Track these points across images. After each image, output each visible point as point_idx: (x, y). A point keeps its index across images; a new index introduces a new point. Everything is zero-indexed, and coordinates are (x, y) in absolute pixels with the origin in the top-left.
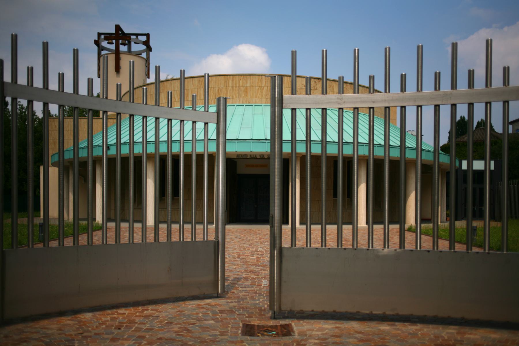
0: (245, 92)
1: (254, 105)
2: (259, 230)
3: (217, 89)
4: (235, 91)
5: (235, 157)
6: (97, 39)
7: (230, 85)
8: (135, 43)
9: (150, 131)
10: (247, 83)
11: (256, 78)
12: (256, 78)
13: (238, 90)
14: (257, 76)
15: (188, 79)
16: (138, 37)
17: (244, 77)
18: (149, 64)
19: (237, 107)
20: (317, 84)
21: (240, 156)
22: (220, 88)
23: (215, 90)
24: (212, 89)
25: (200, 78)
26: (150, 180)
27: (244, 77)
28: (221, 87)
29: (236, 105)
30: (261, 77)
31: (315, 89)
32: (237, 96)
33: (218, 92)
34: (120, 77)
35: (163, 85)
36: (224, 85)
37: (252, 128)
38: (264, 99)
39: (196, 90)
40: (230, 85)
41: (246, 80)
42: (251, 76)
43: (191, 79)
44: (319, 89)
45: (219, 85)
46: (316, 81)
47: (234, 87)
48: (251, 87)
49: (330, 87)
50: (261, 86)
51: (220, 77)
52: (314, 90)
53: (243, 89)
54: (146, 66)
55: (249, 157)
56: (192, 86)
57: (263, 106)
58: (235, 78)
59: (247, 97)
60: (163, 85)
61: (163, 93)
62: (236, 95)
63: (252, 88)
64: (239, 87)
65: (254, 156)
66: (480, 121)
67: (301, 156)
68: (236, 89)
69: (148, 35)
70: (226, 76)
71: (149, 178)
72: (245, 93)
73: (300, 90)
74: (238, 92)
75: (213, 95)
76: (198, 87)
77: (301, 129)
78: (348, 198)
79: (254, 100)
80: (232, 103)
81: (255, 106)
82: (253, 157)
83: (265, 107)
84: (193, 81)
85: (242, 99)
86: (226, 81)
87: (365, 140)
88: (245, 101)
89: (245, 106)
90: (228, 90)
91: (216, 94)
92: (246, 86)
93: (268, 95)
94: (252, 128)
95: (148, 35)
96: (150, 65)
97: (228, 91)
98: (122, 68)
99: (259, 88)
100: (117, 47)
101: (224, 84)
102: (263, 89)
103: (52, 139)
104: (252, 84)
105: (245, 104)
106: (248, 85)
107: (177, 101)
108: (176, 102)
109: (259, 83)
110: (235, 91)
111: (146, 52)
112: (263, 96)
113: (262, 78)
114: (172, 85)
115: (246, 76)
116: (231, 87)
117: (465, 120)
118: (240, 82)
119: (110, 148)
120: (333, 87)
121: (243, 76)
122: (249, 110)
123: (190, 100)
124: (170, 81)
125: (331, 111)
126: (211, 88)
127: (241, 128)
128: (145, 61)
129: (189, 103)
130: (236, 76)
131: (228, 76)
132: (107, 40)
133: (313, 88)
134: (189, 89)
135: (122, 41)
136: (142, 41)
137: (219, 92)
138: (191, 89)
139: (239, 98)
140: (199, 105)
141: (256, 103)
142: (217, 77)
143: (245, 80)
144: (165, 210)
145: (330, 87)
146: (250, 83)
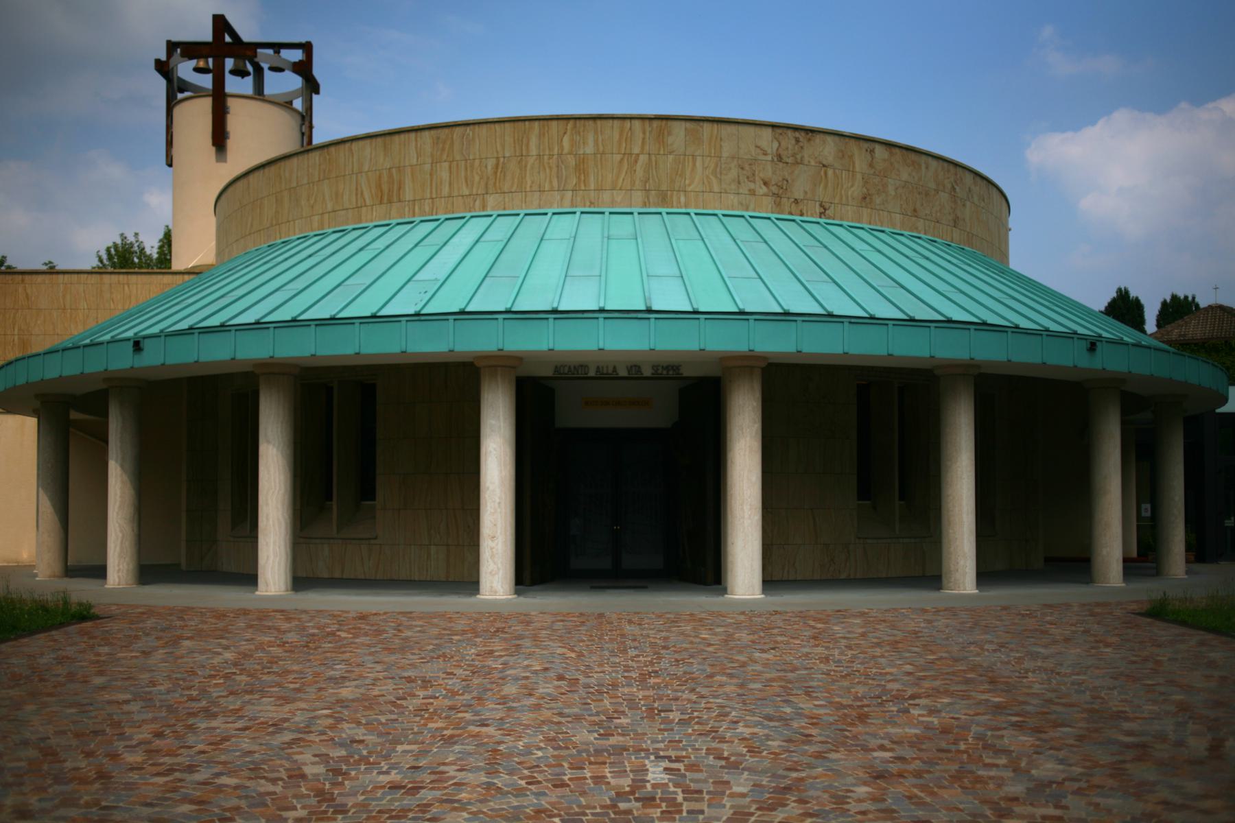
0: (580, 170)
1: (607, 210)
2: (630, 622)
3: (491, 163)
4: (548, 170)
5: (549, 372)
6: (163, 58)
7: (534, 152)
8: (272, 69)
9: (277, 293)
10: (584, 143)
11: (613, 127)
12: (612, 131)
13: (558, 167)
14: (616, 122)
15: (402, 136)
16: (279, 52)
17: (575, 124)
18: (311, 127)
19: (556, 216)
20: (802, 147)
21: (566, 371)
22: (502, 160)
23: (486, 167)
24: (477, 162)
25: (439, 131)
26: (271, 447)
27: (575, 124)
28: (504, 157)
29: (550, 211)
30: (627, 123)
31: (798, 163)
32: (555, 184)
33: (496, 173)
34: (225, 161)
35: (328, 157)
36: (515, 151)
37: (603, 278)
38: (639, 193)
39: (427, 167)
40: (534, 152)
41: (582, 134)
42: (599, 122)
43: (413, 135)
44: (809, 162)
45: (497, 152)
46: (801, 139)
47: (546, 157)
48: (599, 156)
49: (843, 156)
50: (628, 151)
51: (502, 125)
52: (793, 164)
53: (571, 161)
54: (303, 134)
55: (592, 373)
56: (415, 156)
57: (636, 214)
58: (546, 129)
59: (585, 186)
60: (328, 157)
61: (327, 181)
62: (551, 182)
63: (601, 159)
64: (560, 155)
65: (610, 370)
66: (1168, 300)
67: (763, 364)
68: (551, 161)
69: (307, 47)
70: (520, 123)
71: (268, 442)
72: (580, 174)
73: (750, 165)
74: (558, 172)
75: (479, 183)
76: (433, 161)
77: (760, 278)
78: (901, 499)
79: (606, 196)
80: (540, 207)
81: (611, 213)
82: (605, 371)
83: (641, 216)
84: (419, 139)
85: (570, 193)
86: (518, 139)
87: (969, 315)
88: (579, 199)
89: (578, 214)
90: (526, 166)
91: (488, 178)
92: (582, 152)
93: (651, 181)
94: (603, 278)
95: (307, 47)
96: (314, 130)
97: (526, 170)
98: (232, 136)
99: (622, 159)
100: (219, 83)
101: (515, 147)
102: (636, 162)
103: (16, 332)
104: (601, 149)
105: (578, 210)
106: (590, 149)
107: (368, 202)
108: (365, 206)
109: (624, 145)
110: (548, 170)
111: (302, 96)
112: (637, 182)
113: (630, 129)
114: (353, 156)
115: (582, 121)
116: (535, 157)
117: (1129, 297)
118: (562, 140)
119: (141, 345)
120: (851, 157)
121: (571, 123)
122: (592, 226)
123: (407, 199)
124: (348, 145)
125: (847, 229)
126: (474, 159)
127: (566, 276)
128: (299, 118)
129: (407, 209)
130: (550, 122)
131: (527, 123)
132: (191, 58)
133: (791, 158)
134: (404, 166)
135: (235, 64)
136: (289, 62)
137: (498, 174)
138: (411, 166)
139: (562, 190)
140: (436, 214)
141: (613, 203)
142: (492, 126)
143: (580, 135)
144: (332, 541)
145: (843, 156)
146: (596, 142)
